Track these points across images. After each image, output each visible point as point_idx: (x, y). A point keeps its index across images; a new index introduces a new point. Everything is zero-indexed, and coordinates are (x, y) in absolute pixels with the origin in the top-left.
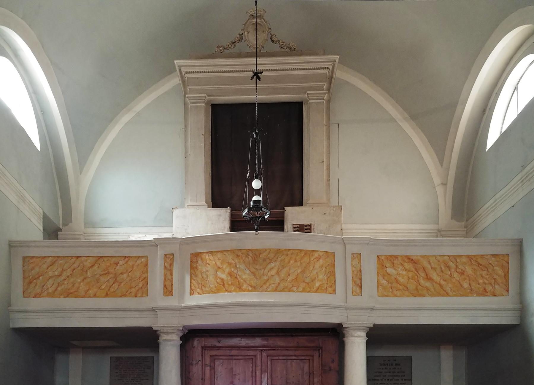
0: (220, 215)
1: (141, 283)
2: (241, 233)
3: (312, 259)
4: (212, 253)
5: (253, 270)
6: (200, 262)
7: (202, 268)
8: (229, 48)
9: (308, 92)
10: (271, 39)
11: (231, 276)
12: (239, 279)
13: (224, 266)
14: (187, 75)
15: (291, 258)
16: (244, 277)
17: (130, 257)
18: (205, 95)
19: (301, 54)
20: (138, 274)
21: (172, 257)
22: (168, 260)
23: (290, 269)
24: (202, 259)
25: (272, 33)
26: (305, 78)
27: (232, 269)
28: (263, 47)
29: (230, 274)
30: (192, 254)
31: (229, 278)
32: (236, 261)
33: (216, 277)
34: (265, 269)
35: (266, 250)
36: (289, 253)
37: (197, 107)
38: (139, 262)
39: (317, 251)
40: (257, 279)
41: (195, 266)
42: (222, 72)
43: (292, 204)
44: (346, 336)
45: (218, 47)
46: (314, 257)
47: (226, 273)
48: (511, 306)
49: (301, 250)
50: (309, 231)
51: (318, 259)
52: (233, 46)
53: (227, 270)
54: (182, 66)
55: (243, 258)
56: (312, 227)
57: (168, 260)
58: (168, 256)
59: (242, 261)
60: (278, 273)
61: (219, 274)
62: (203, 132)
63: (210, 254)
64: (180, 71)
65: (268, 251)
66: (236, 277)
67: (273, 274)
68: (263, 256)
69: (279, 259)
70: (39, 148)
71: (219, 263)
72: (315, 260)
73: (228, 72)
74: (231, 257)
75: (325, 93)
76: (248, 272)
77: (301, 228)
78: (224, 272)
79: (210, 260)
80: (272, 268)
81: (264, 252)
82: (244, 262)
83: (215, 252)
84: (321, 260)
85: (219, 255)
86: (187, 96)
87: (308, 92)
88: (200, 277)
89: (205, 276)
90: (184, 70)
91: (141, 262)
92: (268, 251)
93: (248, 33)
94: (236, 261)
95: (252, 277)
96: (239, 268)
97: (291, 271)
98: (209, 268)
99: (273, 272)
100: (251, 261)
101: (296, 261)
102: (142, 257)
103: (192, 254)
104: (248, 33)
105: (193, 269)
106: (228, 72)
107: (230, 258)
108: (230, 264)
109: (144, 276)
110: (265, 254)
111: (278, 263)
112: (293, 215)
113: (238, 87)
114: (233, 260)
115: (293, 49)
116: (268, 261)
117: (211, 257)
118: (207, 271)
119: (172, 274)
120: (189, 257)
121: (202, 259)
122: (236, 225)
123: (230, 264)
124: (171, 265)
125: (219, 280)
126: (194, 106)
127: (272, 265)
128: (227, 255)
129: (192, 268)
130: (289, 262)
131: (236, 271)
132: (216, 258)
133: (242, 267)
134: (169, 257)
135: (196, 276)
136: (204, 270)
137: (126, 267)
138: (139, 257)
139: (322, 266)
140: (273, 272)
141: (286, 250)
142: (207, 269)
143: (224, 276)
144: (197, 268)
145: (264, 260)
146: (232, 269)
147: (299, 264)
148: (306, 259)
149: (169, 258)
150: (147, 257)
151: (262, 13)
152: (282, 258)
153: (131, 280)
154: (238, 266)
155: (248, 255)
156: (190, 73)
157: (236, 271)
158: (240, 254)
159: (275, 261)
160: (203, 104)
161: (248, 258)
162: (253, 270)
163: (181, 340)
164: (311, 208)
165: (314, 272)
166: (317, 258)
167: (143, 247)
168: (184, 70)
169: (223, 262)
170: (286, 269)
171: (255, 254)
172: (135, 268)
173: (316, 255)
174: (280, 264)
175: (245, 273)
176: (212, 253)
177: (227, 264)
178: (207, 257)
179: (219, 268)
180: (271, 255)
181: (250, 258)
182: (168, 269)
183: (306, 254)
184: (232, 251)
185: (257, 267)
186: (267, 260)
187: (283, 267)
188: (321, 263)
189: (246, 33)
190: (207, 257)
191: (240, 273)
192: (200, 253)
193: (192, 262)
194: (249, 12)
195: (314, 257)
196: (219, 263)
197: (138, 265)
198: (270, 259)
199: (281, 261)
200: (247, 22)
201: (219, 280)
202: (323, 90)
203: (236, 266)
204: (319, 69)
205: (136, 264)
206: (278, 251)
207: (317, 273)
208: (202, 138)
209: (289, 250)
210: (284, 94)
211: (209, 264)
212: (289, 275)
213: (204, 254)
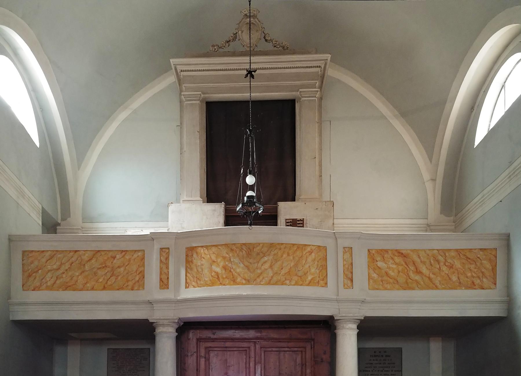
0: (214, 210)
1: (138, 276)
2: (235, 228)
3: (304, 253)
4: (207, 247)
5: (247, 263)
6: (195, 255)
7: (197, 261)
8: (223, 47)
9: (300, 90)
10: (264, 38)
11: (225, 269)
12: (234, 273)
13: (219, 260)
14: (182, 73)
15: (284, 252)
16: (238, 270)
17: (127, 251)
18: (200, 93)
19: (294, 53)
20: (134, 268)
21: (167, 251)
22: (164, 254)
23: (283, 263)
24: (197, 253)
25: (266, 33)
26: (298, 77)
27: (227, 263)
28: (256, 46)
29: (225, 268)
30: (187, 248)
31: (224, 272)
32: (231, 255)
33: (211, 270)
34: (258, 262)
35: (259, 244)
36: (282, 247)
37: (192, 104)
38: (135, 256)
39: (310, 245)
40: (251, 272)
41: (190, 260)
42: (217, 70)
43: (285, 199)
44: (337, 328)
45: (212, 46)
46: (307, 251)
47: (221, 266)
48: (499, 299)
49: (294, 245)
50: (301, 225)
51: (311, 252)
52: (227, 44)
53: (222, 264)
54: (177, 65)
55: (238, 252)
56: (305, 222)
57: (164, 254)
58: (164, 250)
59: (236, 255)
60: (271, 267)
61: (214, 267)
62: (198, 128)
63: (205, 248)
64: (176, 69)
65: (261, 245)
66: (230, 271)
67: (266, 268)
68: (257, 250)
69: (273, 253)
70: (38, 144)
71: (213, 257)
72: (308, 254)
73: (222, 70)
74: (225, 251)
75: (318, 91)
76: (242, 265)
77: (294, 223)
78: (218, 265)
79: (205, 254)
80: (265, 262)
81: (257, 246)
82: (238, 255)
83: (210, 246)
84: (313, 254)
85: (214, 249)
86: (182, 93)
87: (300, 90)
88: (195, 270)
89: (200, 270)
90: (179, 68)
91: (138, 256)
92: (261, 245)
93: (242, 32)
94: (231, 255)
95: (246, 270)
96: (234, 261)
97: (284, 265)
98: (204, 262)
99: (267, 266)
100: (245, 255)
101: (288, 255)
102: (139, 251)
103: (187, 248)
104: (242, 32)
105: (189, 262)
106: (222, 70)
107: (224, 252)
108: (224, 258)
109: (141, 269)
110: (258, 248)
111: (271, 257)
112: (286, 210)
113: (232, 85)
114: (228, 254)
115: (286, 48)
116: (262, 255)
117: (206, 251)
118: (202, 265)
119: (167, 268)
120: (184, 251)
121: (197, 253)
122: (230, 219)
123: (224, 258)
124: (167, 259)
125: (213, 274)
126: (189, 104)
127: (266, 259)
128: (222, 249)
129: (187, 262)
130: (282, 256)
131: (230, 265)
132: (211, 252)
133: (237, 260)
134: (165, 251)
135: (191, 269)
136: (199, 264)
137: (123, 261)
138: (135, 251)
139: (314, 260)
140: (267, 266)
141: (279, 244)
142: (202, 263)
143: (218, 270)
144: (192, 262)
145: (258, 254)
146: (227, 263)
147: (291, 258)
148: (298, 253)
149: (165, 252)
150: (144, 251)
151: (255, 12)
152: (276, 252)
153: (127, 273)
154: (232, 260)
155: (242, 249)
156: (185, 71)
157: (230, 265)
158: (234, 248)
159: (269, 255)
160: (198, 102)
161: (242, 252)
162: (247, 263)
163: (176, 332)
164: (303, 203)
165: (307, 266)
166: (309, 252)
167: (140, 241)
168: (179, 68)
169: (217, 256)
170: (279, 263)
171: (249, 248)
172: (132, 262)
173: (309, 249)
174: (273, 258)
175: (239, 267)
176: (207, 247)
177: (221, 258)
178: (202, 251)
179: (214, 262)
180: (265, 249)
181: (244, 252)
182: (164, 263)
183: (298, 248)
184: (226, 245)
185: (251, 261)
186: (261, 254)
187: (276, 261)
188: (313, 257)
189: (240, 32)
190: (202, 251)
191: (234, 267)
192: (196, 247)
193: (187, 256)
194: (243, 11)
195: (307, 251)
196: (213, 257)
197: (135, 259)
198: (263, 253)
199: (274, 255)
200: (241, 22)
201: (213, 274)
202: (315, 88)
203: (230, 260)
204: (311, 67)
205: (133, 258)
206: (271, 246)
207: (309, 267)
208: (197, 135)
209: (282, 244)
210: (277, 92)
211: (204, 258)
212: (282, 269)
213: (200, 248)
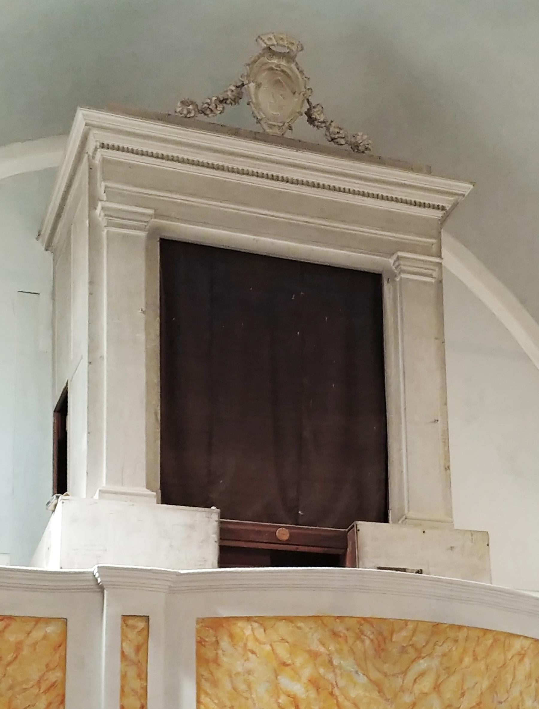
0: (192, 527)
1: (44, 697)
2: (322, 572)
3: (509, 656)
4: (261, 621)
5: (375, 675)
6: (225, 643)
7: (231, 659)
8: (208, 112)
9: (400, 254)
10: (308, 114)
11: (318, 689)
12: (341, 699)
13: (299, 661)
15: (465, 651)
16: (353, 693)
17: (10, 618)
18: (150, 212)
19: (380, 161)
20: (34, 672)
21: (141, 625)
22: (132, 635)
23: (463, 680)
24: (231, 636)
25: (314, 103)
26: (390, 221)
27: (322, 671)
28: (290, 128)
29: (315, 683)
30: (200, 621)
31: (313, 694)
32: (332, 648)
33: (276, 690)
34: (405, 673)
35: (406, 622)
36: (462, 635)
37: (125, 236)
38: (37, 634)
39: (519, 636)
40: (387, 700)
41: (210, 654)
42: (198, 164)
45: (182, 103)
46: (513, 651)
47: (304, 679)
49: (486, 631)
51: (522, 656)
52: (220, 108)
53: (307, 672)
54: (94, 126)
55: (350, 641)
57: (132, 635)
58: (131, 622)
59: (346, 648)
60: (437, 688)
61: (285, 681)
62: (141, 302)
63: (256, 625)
65: (411, 626)
66: (332, 694)
67: (426, 690)
68: (400, 637)
69: (439, 650)
71: (282, 651)
72: (516, 659)
73: (212, 167)
74: (316, 636)
76: (362, 679)
78: (296, 676)
79: (257, 640)
80: (422, 674)
81: (401, 629)
82: (352, 651)
83: (270, 618)
84: (527, 661)
85: (283, 628)
87: (400, 254)
88: (228, 686)
89: (242, 687)
91: (45, 638)
92: (411, 626)
93: (259, 86)
94: (332, 648)
95: (375, 695)
96: (340, 667)
97: (468, 684)
98: (254, 663)
99: (426, 684)
100: (371, 652)
101: (475, 659)
102: (48, 620)
103: (200, 621)
104: (259, 86)
105: (206, 661)
106: (212, 167)
107: (314, 639)
108: (314, 655)
109: (54, 676)
110: (404, 633)
111: (435, 662)
113: (231, 208)
114: (323, 645)
115: (361, 148)
116: (412, 654)
117: (260, 633)
118: (249, 672)
119: (143, 675)
120: (193, 626)
121: (231, 636)
122: (231, 554)
123: (314, 655)
124: (142, 648)
125: (283, 700)
126: (119, 234)
127: (423, 664)
128: (307, 629)
129: (202, 660)
130: (461, 660)
131: (330, 676)
132: (275, 637)
133: (348, 664)
134: (136, 627)
135: (215, 684)
136: (240, 669)
138: (38, 620)
139: (529, 677)
140: (426, 684)
141: (452, 626)
142: (250, 665)
143: (298, 689)
144: (216, 661)
145: (403, 650)
146: (322, 671)
147: (482, 665)
148: (497, 656)
149: (134, 627)
150: (65, 621)
151: (294, 48)
152: (446, 647)
153: (11, 688)
154: (335, 662)
155: (362, 632)
156: (113, 148)
157: (330, 676)
158: (340, 628)
159: (430, 655)
161: (363, 641)
162: (375, 675)
164: (420, 531)
165: (515, 692)
166: (519, 654)
167: (53, 590)
169: (294, 648)
170: (455, 679)
171: (381, 633)
172: (26, 651)
173: (517, 645)
174: (441, 664)
175: (355, 684)
176: (261, 621)
177: (306, 656)
178: (248, 632)
179: (285, 664)
180: (420, 639)
181: (367, 642)
182: (134, 662)
183: (496, 641)
184: (318, 619)
185: (386, 667)
186: (410, 650)
187: (449, 671)
188: (528, 669)
189: (252, 85)
190: (248, 632)
191: (342, 683)
192: (227, 619)
193: (200, 643)
194: (265, 38)
195: (513, 651)
196: (282, 651)
197: (34, 645)
198: (416, 649)
199: (444, 655)
200: (255, 62)
201: (283, 700)
203: (331, 662)
204: (424, 205)
205: (29, 641)
206: (436, 629)
207: (521, 694)
208: (140, 318)
209: (460, 627)
210: (342, 247)
211: (253, 652)
212: (463, 695)
213: (240, 624)
